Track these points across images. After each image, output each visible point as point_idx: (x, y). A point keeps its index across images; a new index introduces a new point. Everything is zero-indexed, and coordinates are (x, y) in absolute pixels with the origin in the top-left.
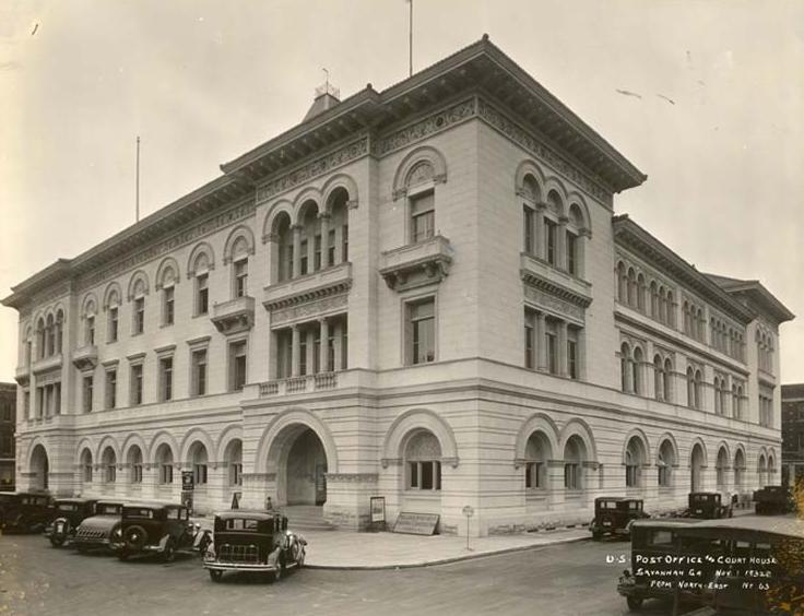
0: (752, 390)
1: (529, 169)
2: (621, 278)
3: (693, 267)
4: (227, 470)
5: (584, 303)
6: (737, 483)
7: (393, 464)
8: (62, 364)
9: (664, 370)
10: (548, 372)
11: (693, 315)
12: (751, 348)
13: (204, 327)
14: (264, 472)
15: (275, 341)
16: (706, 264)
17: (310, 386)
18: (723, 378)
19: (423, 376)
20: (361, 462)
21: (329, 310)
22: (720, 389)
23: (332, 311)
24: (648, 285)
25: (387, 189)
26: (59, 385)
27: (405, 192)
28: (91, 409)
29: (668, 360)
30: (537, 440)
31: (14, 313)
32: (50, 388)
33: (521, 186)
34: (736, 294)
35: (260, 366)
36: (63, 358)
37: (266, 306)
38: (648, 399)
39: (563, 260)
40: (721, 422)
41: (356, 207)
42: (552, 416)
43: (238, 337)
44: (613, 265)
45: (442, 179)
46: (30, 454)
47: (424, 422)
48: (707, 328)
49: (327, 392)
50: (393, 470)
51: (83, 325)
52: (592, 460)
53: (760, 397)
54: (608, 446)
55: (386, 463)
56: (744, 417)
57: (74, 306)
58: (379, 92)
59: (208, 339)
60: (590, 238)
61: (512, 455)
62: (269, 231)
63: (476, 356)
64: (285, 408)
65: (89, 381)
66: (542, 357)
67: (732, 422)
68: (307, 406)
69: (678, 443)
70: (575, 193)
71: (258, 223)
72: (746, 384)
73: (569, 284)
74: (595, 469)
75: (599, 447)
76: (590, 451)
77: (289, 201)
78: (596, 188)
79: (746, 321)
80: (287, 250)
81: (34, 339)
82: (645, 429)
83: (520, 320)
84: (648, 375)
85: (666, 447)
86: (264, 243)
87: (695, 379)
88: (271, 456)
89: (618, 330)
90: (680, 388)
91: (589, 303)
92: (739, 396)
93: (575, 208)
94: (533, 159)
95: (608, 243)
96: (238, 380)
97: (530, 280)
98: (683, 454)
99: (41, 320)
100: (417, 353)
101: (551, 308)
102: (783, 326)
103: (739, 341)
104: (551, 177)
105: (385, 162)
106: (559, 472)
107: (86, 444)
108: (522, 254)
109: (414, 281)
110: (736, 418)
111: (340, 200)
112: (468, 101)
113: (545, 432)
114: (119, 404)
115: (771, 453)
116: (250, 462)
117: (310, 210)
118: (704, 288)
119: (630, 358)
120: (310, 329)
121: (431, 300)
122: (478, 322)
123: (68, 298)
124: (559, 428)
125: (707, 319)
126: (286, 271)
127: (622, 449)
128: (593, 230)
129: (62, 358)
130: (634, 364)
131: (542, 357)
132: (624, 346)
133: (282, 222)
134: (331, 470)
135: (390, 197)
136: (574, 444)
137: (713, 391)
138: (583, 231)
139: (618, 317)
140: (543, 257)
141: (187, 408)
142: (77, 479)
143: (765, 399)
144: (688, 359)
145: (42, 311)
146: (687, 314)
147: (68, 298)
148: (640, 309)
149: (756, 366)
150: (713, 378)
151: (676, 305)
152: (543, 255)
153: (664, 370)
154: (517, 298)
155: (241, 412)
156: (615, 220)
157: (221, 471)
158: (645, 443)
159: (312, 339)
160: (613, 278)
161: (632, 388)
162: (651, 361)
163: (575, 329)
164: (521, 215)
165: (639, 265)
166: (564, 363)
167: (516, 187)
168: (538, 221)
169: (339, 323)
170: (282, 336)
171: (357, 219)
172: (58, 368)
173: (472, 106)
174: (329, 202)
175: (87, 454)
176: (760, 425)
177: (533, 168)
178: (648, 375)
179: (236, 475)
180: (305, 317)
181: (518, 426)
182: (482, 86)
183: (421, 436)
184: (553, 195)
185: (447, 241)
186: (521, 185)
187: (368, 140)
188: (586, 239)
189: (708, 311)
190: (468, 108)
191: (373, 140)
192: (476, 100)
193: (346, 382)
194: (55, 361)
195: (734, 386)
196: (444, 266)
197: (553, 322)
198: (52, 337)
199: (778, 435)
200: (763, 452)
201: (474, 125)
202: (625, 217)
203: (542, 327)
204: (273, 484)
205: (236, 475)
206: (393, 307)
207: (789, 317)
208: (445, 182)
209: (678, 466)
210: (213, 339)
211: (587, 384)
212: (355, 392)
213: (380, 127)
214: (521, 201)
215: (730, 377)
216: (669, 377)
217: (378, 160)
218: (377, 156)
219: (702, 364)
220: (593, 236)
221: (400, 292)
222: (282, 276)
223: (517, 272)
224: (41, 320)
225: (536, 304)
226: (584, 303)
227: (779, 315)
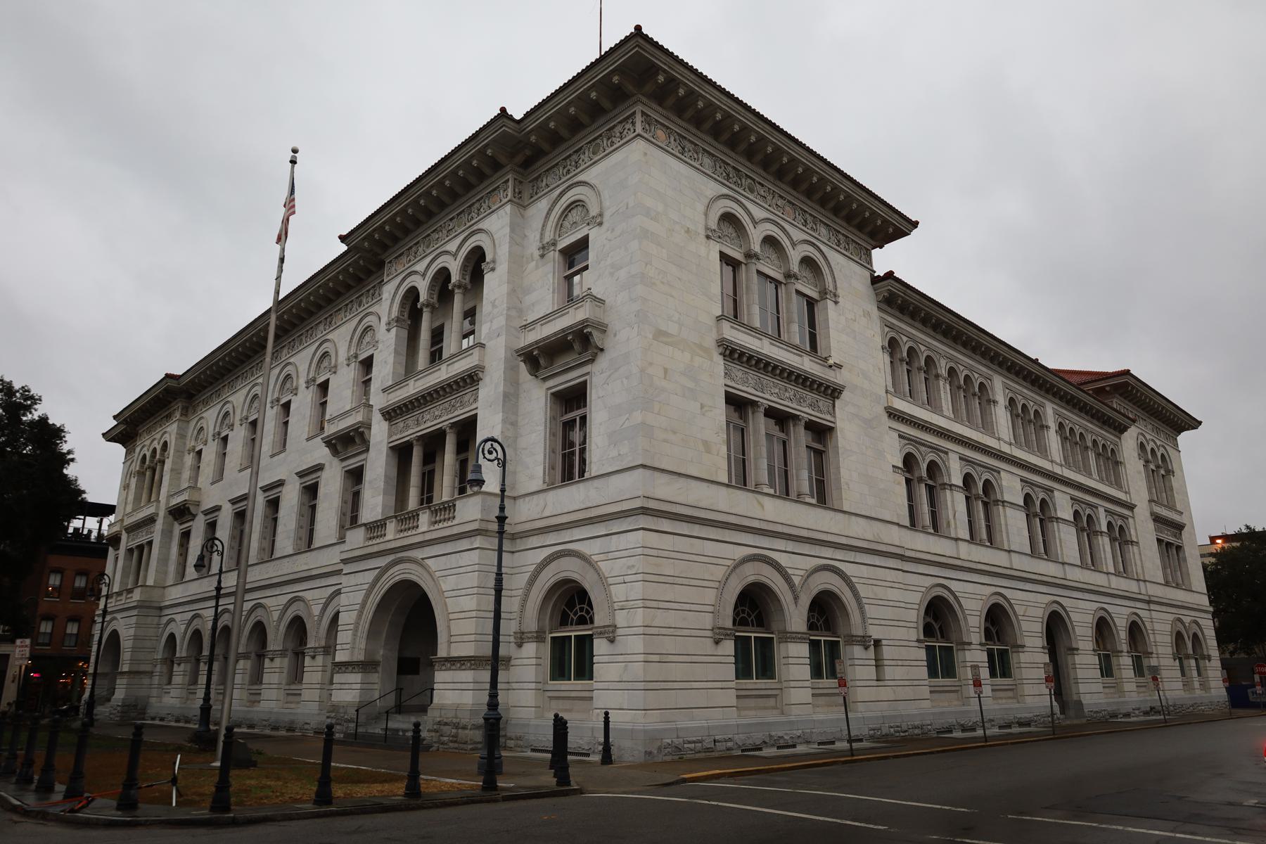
0: (1143, 530)
3: (1036, 361)
7: (530, 640)
8: (157, 514)
10: (814, 501)
11: (1026, 419)
12: (1133, 467)
13: (320, 453)
14: (362, 658)
15: (394, 462)
16: (1056, 355)
18: (1042, 495)
19: (573, 498)
21: (456, 413)
22: (1084, 525)
23: (460, 414)
24: (1090, 444)
25: (533, 249)
27: (554, 244)
28: (183, 576)
29: (1089, 516)
30: (754, 604)
31: (119, 450)
32: (433, 444)
33: (714, 227)
34: (1100, 392)
35: (374, 504)
37: (383, 415)
38: (957, 539)
39: (796, 331)
41: (493, 269)
42: (782, 559)
43: (353, 463)
49: (444, 530)
51: (189, 459)
52: (860, 633)
53: (1159, 541)
56: (1136, 568)
57: (181, 436)
58: (518, 116)
59: (319, 468)
60: (836, 303)
61: (707, 621)
62: (395, 313)
63: (640, 463)
64: (391, 557)
66: (760, 469)
67: (1113, 578)
69: (1074, 616)
70: (767, 220)
72: (1131, 520)
73: (806, 364)
74: (866, 648)
75: (871, 611)
76: (855, 617)
77: (415, 273)
78: (809, 219)
79: (1121, 429)
81: (133, 481)
82: (954, 586)
83: (720, 410)
84: (955, 504)
85: (997, 619)
86: (388, 330)
88: (372, 633)
89: (896, 435)
91: (840, 393)
92: (1121, 538)
93: (770, 241)
94: (731, 193)
95: (867, 314)
97: (732, 353)
98: (1031, 632)
99: (145, 456)
100: (570, 464)
102: (1184, 438)
103: (1111, 461)
104: (761, 216)
105: (532, 211)
106: (801, 650)
107: (172, 628)
108: (719, 319)
111: (476, 263)
112: (628, 118)
113: (836, 590)
115: (1195, 628)
119: (921, 476)
122: (663, 395)
123: (175, 426)
124: (797, 580)
125: (1051, 422)
127: (914, 616)
128: (839, 292)
129: (158, 508)
130: (1041, 520)
131: (760, 469)
133: (411, 306)
134: (442, 652)
135: (537, 253)
136: (825, 610)
137: (1073, 530)
138: (824, 293)
139: (893, 414)
140: (797, 341)
142: (156, 680)
143: (1169, 545)
144: (900, 436)
145: (147, 444)
146: (1064, 439)
147: (175, 426)
148: (932, 403)
149: (1146, 496)
150: (1072, 513)
151: (1048, 427)
154: (715, 377)
155: (339, 572)
156: (875, 280)
158: (956, 606)
161: (984, 536)
162: (1104, 529)
163: (821, 432)
165: (927, 343)
166: (802, 479)
167: (707, 228)
168: (748, 276)
170: (402, 453)
171: (494, 285)
173: (633, 124)
174: (464, 267)
176: (1167, 584)
177: (811, 249)
178: (955, 504)
181: (719, 573)
182: (637, 85)
184: (770, 242)
185: (602, 301)
186: (713, 224)
187: (510, 184)
188: (830, 303)
189: (1050, 412)
190: (627, 126)
191: (519, 182)
192: (639, 119)
195: (1109, 524)
196: (596, 334)
197: (781, 419)
199: (1204, 601)
200: (1180, 627)
201: (639, 145)
202: (890, 275)
203: (760, 425)
204: (375, 677)
207: (1194, 424)
208: (600, 224)
209: (1023, 646)
210: (327, 467)
211: (835, 510)
212: (475, 526)
214: (715, 249)
215: (1101, 510)
216: (1050, 525)
217: (525, 207)
218: (521, 202)
219: (1050, 490)
220: (840, 300)
221: (545, 379)
222: (409, 370)
223: (1148, 514)
224: (145, 456)
225: (748, 387)
226: (832, 392)
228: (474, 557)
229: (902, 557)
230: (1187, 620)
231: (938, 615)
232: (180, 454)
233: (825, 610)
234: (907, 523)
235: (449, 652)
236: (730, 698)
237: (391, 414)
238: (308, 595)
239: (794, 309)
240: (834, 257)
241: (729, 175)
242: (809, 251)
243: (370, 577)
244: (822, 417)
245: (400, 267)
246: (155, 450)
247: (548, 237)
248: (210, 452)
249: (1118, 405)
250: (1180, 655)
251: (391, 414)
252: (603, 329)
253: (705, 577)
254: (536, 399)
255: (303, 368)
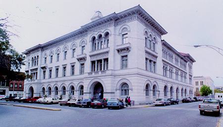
0: (188, 76)
1: (146, 30)
2: (163, 52)
4: (120, 91)
5: (156, 57)
6: (154, 94)
9: (171, 72)
11: (177, 60)
16: (179, 50)
17: (100, 73)
20: (112, 90)
23: (105, 57)
26: (37, 73)
30: (147, 86)
32: (34, 73)
36: (39, 66)
39: (152, 49)
40: (182, 83)
42: (128, 78)
43: (82, 63)
44: (161, 49)
45: (130, 31)
46: (90, 86)
47: (125, 81)
48: (179, 63)
49: (104, 74)
50: (118, 91)
51: (44, 59)
54: (160, 87)
55: (116, 90)
57: (41, 55)
59: (75, 63)
65: (45, 72)
68: (99, 78)
71: (88, 38)
79: (187, 62)
80: (94, 44)
84: (168, 72)
87: (177, 74)
88: (90, 89)
90: (174, 75)
92: (185, 78)
93: (150, 35)
96: (82, 72)
97: (147, 52)
98: (175, 90)
100: (124, 65)
101: (150, 58)
102: (193, 63)
103: (185, 66)
104: (150, 31)
106: (152, 92)
109: (123, 52)
110: (185, 82)
111: (107, 34)
114: (52, 77)
116: (85, 90)
117: (100, 36)
118: (178, 55)
119: (165, 69)
120: (100, 61)
121: (127, 56)
122: (137, 58)
126: (94, 49)
127: (163, 88)
132: (164, 67)
133: (94, 38)
134: (104, 91)
136: (154, 87)
139: (163, 61)
141: (54, 80)
152: (149, 47)
153: (171, 72)
154: (144, 56)
157: (78, 92)
159: (100, 63)
160: (162, 52)
163: (155, 63)
164: (145, 39)
168: (152, 42)
169: (106, 60)
170: (93, 62)
171: (111, 38)
172: (37, 69)
175: (44, 89)
179: (82, 93)
180: (99, 58)
182: (139, 13)
183: (125, 84)
193: (108, 72)
194: (35, 67)
197: (150, 61)
198: (35, 62)
205: (82, 93)
206: (119, 57)
213: (116, 20)
225: (148, 57)
226: (156, 57)
227: (192, 61)
228: (110, 79)
229: (145, 76)
230: (152, 81)
231: (166, 87)
232: (41, 58)
233: (154, 87)
234: (145, 69)
235: (105, 93)
236: (145, 98)
237: (91, 56)
238: (74, 82)
239: (152, 45)
240: (158, 37)
241: (146, 25)
242: (150, 33)
243: (90, 80)
244: (155, 61)
245: (92, 32)
246: (35, 57)
247: (120, 32)
248: (49, 58)
249: (187, 59)
250: (190, 93)
251: (91, 56)
252: (130, 48)
253: (143, 83)
254: (119, 56)
255: (70, 46)
